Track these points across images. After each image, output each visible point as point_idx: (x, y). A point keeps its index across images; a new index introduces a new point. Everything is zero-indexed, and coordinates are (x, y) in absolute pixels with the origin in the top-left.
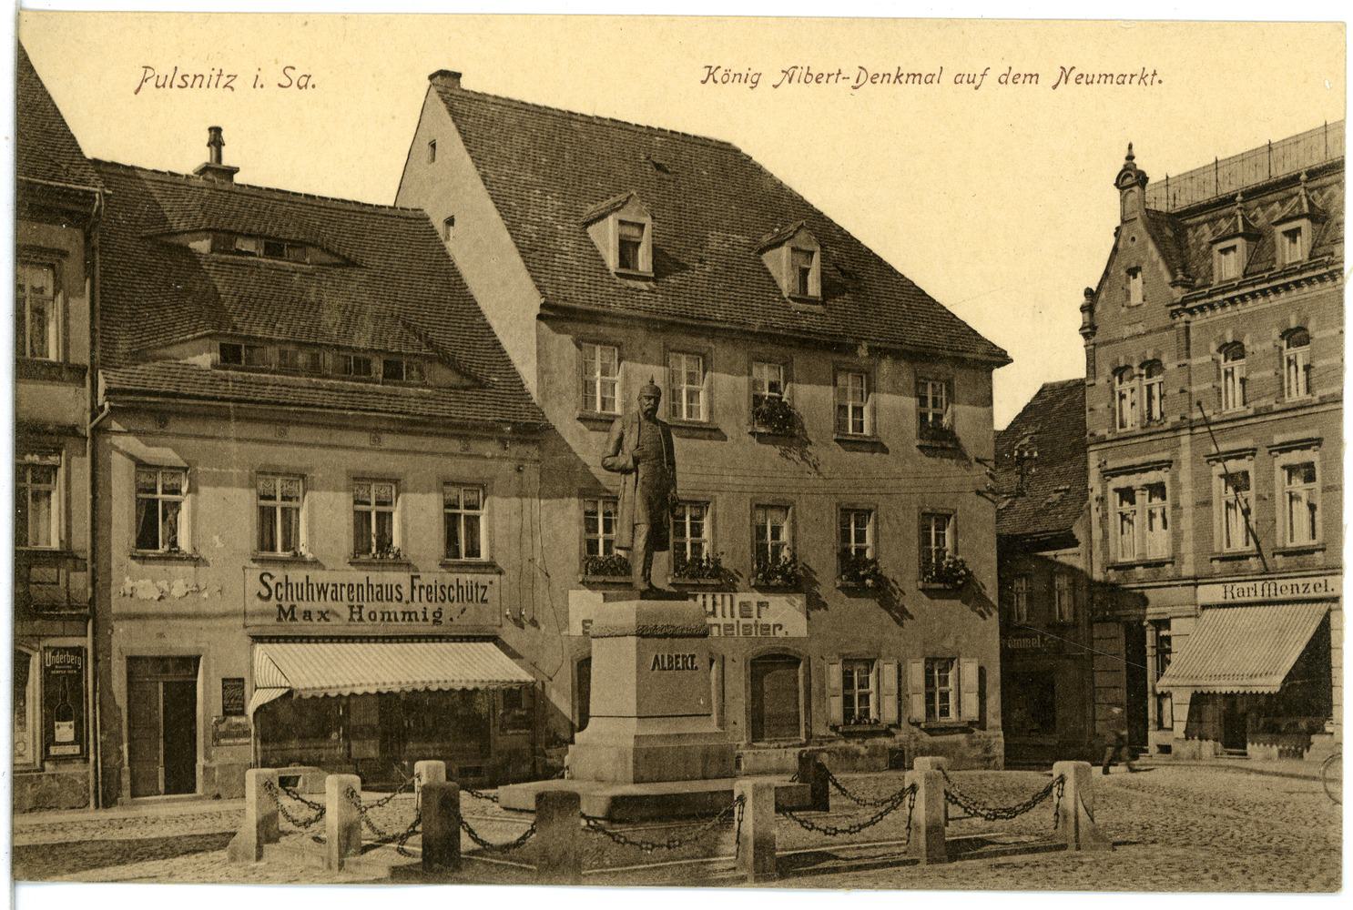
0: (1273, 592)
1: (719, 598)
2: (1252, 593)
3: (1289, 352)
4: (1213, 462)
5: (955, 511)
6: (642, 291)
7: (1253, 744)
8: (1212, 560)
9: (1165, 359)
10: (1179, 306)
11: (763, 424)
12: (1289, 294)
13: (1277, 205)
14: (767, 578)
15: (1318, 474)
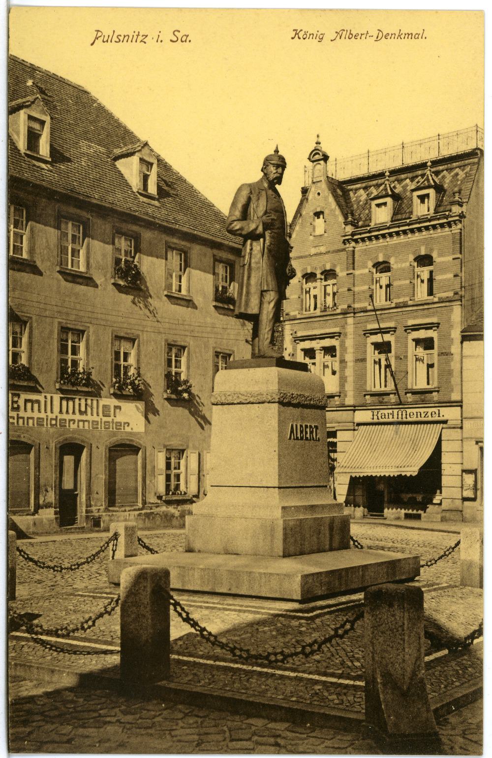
0: (404, 416)
1: (89, 402)
2: (391, 416)
3: (418, 270)
4: (368, 335)
5: (234, 352)
6: (43, 169)
7: (388, 509)
8: (365, 395)
9: (338, 270)
10: (350, 237)
11: (121, 278)
12: (421, 234)
13: (408, 181)
14: (120, 388)
15: (436, 346)
